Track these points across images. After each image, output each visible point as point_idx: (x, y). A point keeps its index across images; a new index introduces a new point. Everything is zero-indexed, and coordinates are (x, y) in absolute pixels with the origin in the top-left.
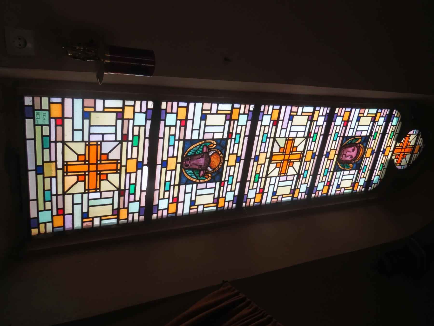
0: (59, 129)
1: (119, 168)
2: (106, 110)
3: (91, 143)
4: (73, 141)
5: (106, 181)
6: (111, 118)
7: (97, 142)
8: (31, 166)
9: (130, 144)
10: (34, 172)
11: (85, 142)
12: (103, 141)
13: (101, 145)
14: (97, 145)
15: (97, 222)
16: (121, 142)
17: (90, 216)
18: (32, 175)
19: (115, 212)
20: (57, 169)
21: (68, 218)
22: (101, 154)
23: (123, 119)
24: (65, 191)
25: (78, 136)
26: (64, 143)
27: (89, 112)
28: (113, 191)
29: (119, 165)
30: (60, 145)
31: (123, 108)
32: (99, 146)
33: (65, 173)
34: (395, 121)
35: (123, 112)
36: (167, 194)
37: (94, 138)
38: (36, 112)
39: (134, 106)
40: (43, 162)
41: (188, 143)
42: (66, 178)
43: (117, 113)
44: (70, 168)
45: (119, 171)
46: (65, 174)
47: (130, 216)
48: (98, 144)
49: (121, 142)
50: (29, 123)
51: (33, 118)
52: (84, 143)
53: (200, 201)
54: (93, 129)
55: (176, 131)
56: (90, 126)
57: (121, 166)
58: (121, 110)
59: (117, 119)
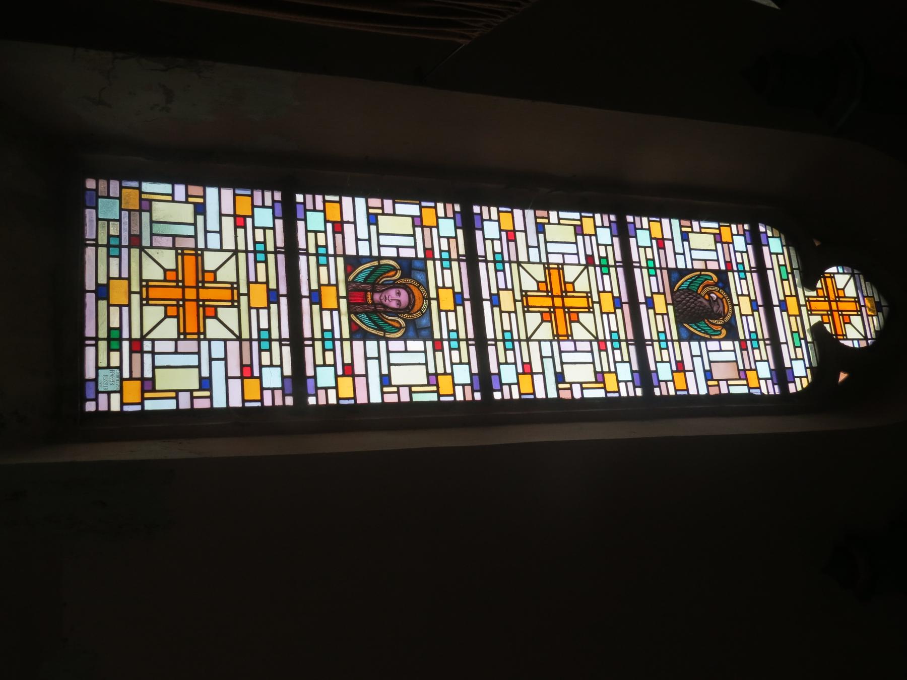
0: (246, 361)
1: (236, 298)
2: (173, 394)
3: (196, 337)
4: (225, 341)
5: (215, 320)
6: (164, 380)
7: (185, 339)
8: (90, 284)
9: (125, 335)
10: (93, 295)
11: (205, 339)
12: (176, 341)
13: (179, 333)
14: (185, 334)
15: (180, 190)
16: (143, 338)
17: (191, 207)
18: (90, 299)
19: (145, 205)
20: (339, 297)
21: (228, 208)
22: (177, 317)
23: (142, 379)
24: (144, 334)
25: (218, 350)
26: (239, 338)
27: (201, 389)
28: (151, 247)
29: (144, 296)
30: (245, 335)
31: (143, 399)
32: (182, 331)
33: (235, 288)
34: (776, 245)
35: (143, 391)
36: (329, 355)
37: (192, 346)
38: (100, 200)
39: (122, 404)
40: (109, 278)
41: (352, 262)
42: (144, 308)
43: (154, 390)
44: (532, 301)
45: (144, 283)
46: (144, 302)
47: (267, 395)
48: (183, 334)
49: (143, 338)
50: (90, 214)
51: (96, 208)
52: (208, 337)
53: (399, 376)
54: (193, 360)
55: (328, 239)
56: (199, 367)
57: (239, 295)
58: (147, 395)
59: (153, 379)
